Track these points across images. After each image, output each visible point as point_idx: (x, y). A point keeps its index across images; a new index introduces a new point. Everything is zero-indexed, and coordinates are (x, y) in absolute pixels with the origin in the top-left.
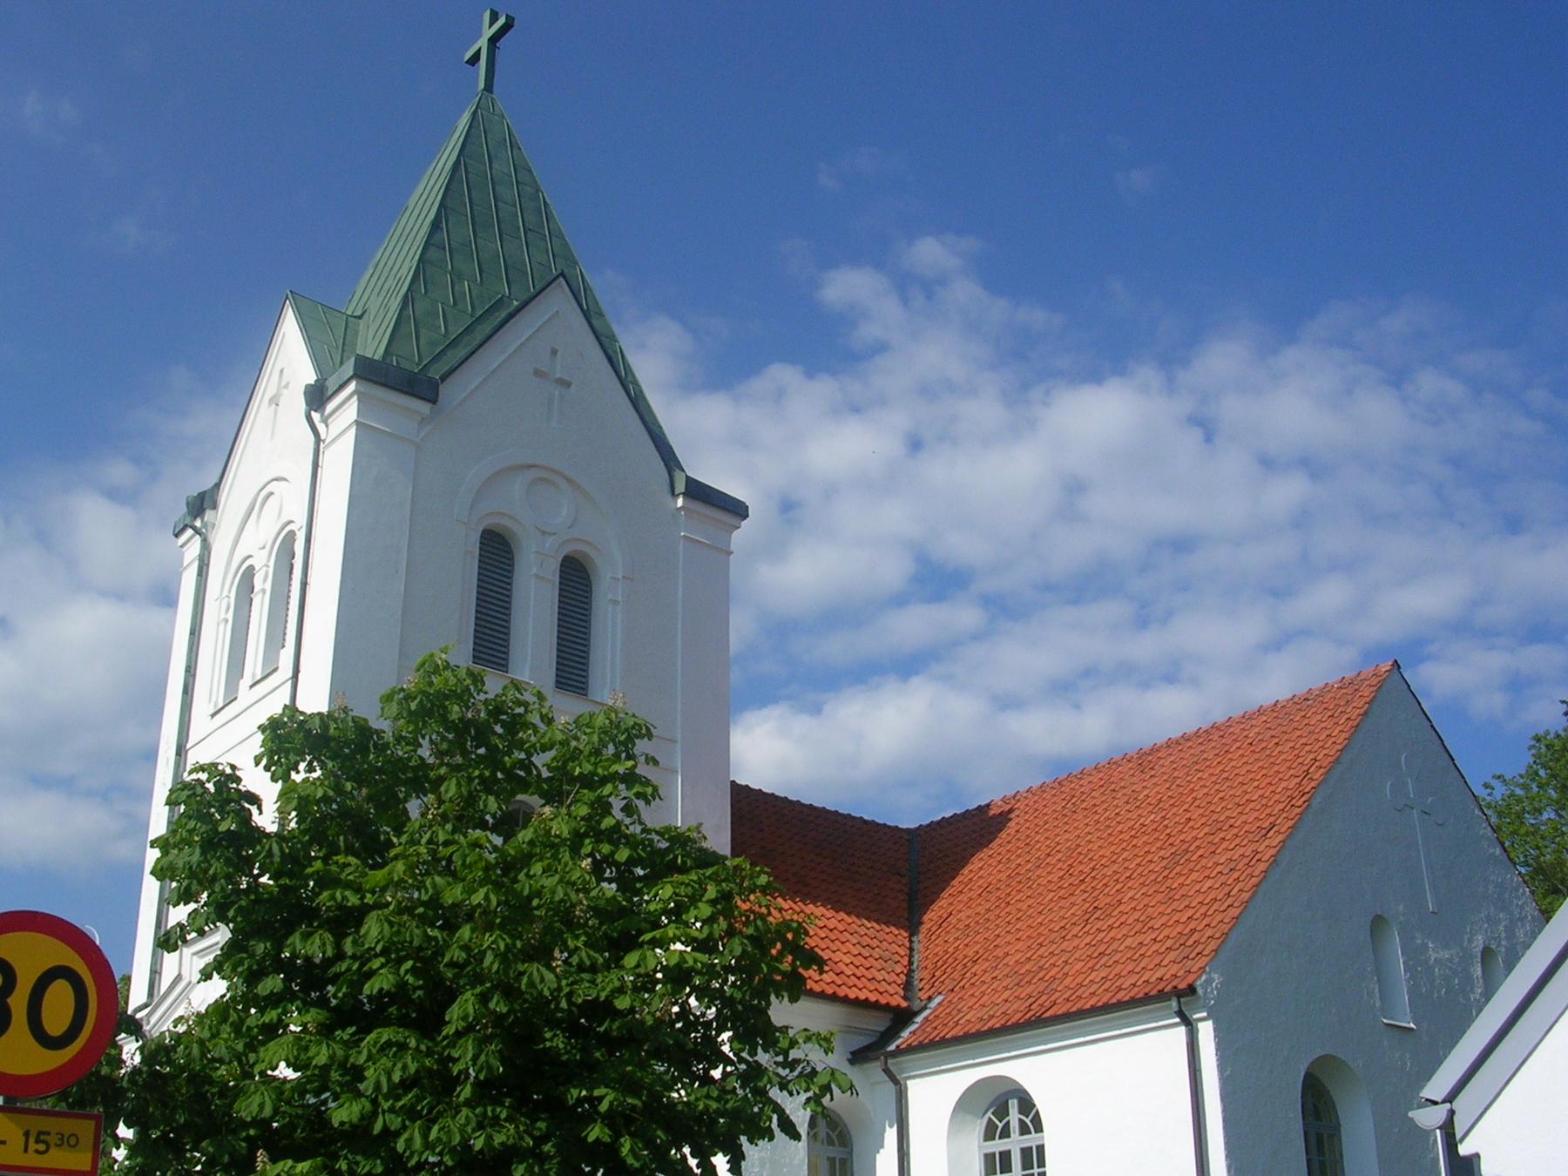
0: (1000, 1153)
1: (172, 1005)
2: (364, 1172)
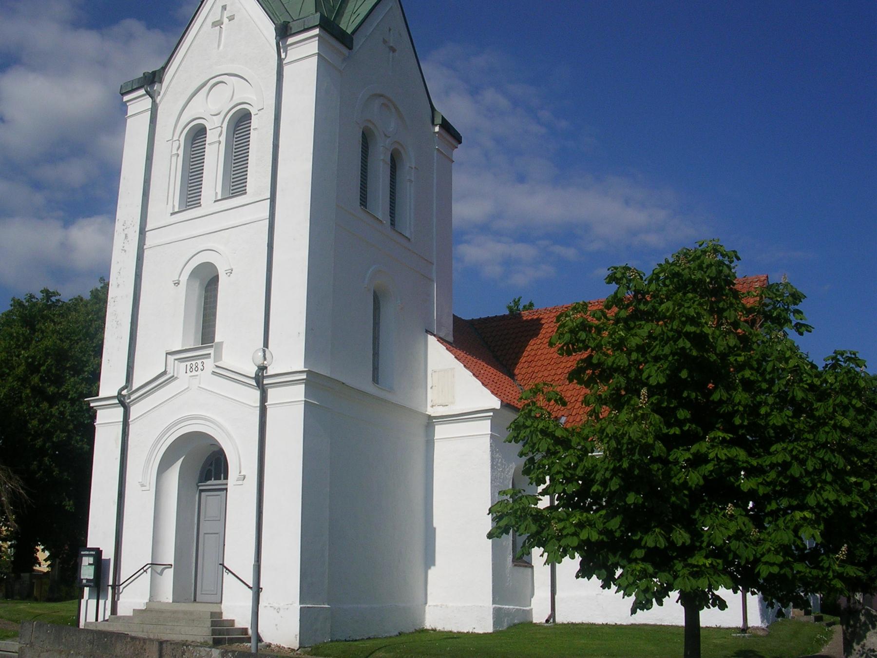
0: (220, 479)
1: (153, 389)
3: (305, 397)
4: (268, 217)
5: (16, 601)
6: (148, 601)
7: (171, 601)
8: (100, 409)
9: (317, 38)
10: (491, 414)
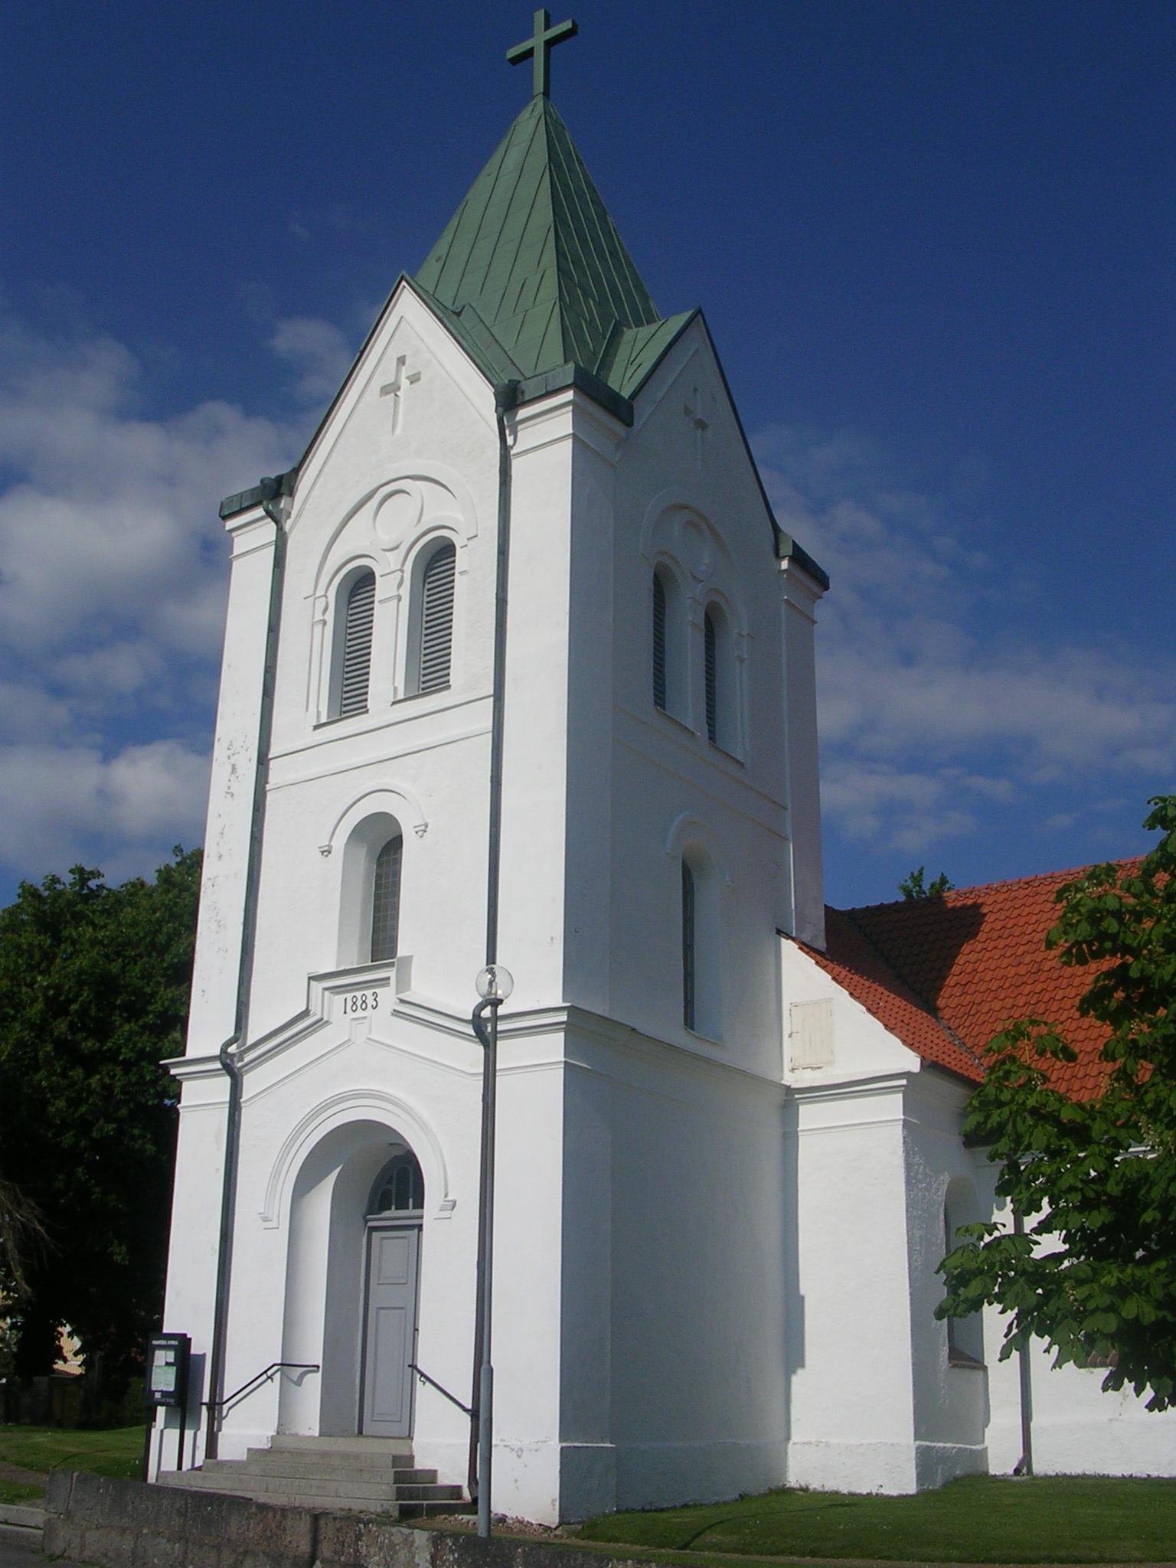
0: (408, 1208)
1: (270, 1051)
3: (565, 1057)
4: (491, 729)
5: (25, 1427)
6: (274, 1434)
7: (317, 1434)
8: (188, 1079)
9: (571, 408)
10: (904, 1082)
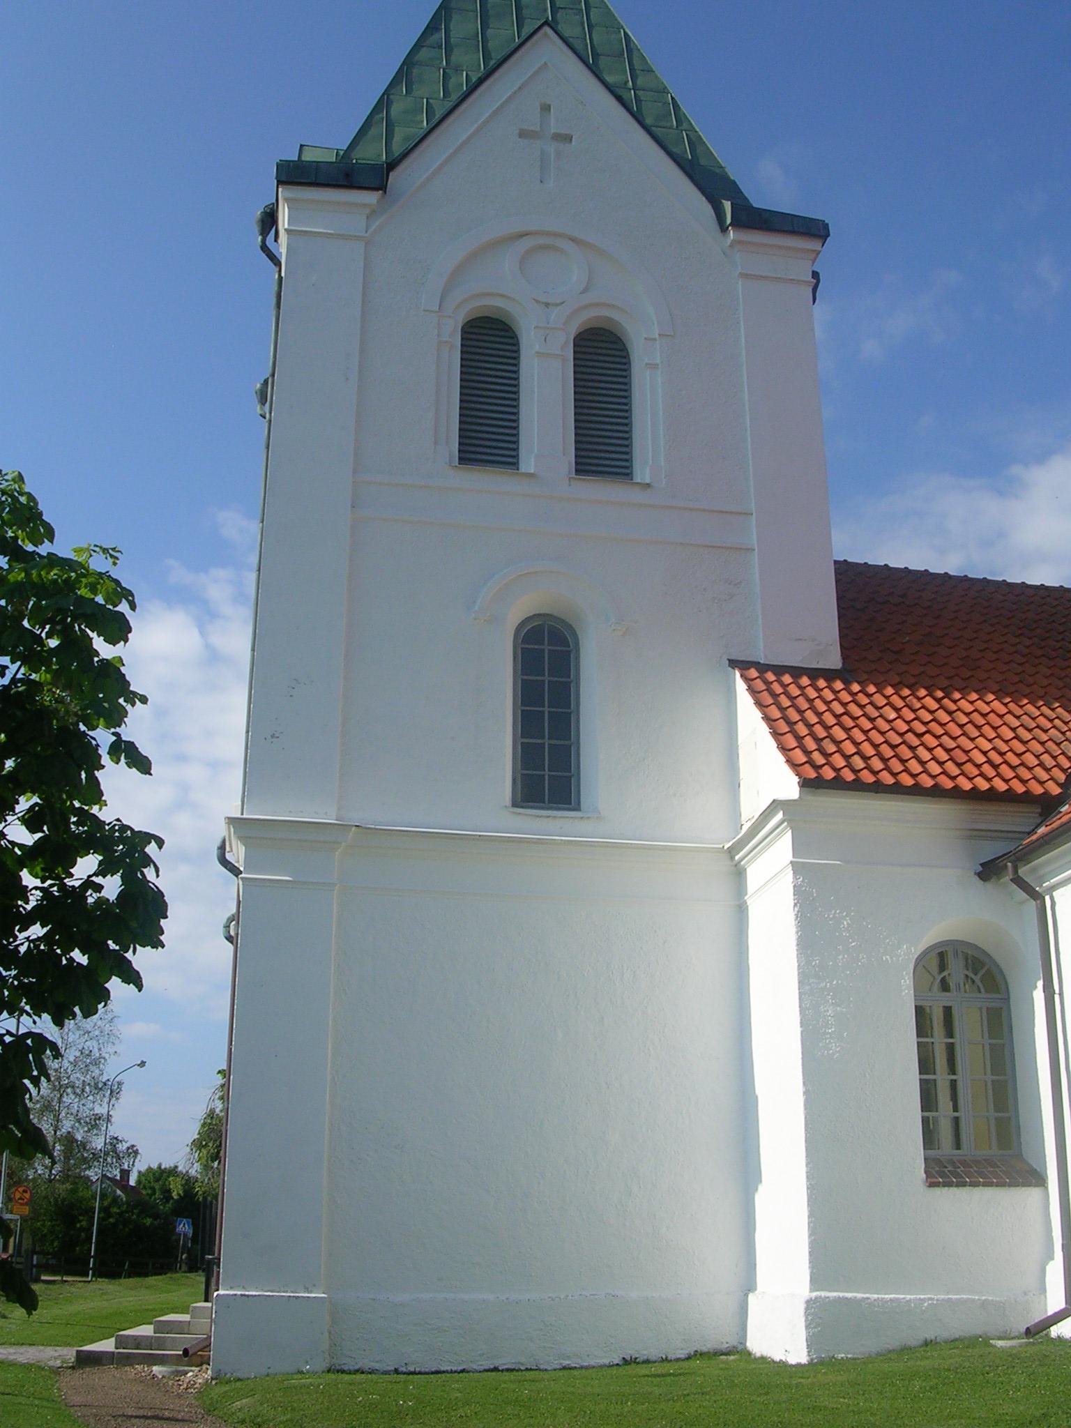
2: (5, 1154)
